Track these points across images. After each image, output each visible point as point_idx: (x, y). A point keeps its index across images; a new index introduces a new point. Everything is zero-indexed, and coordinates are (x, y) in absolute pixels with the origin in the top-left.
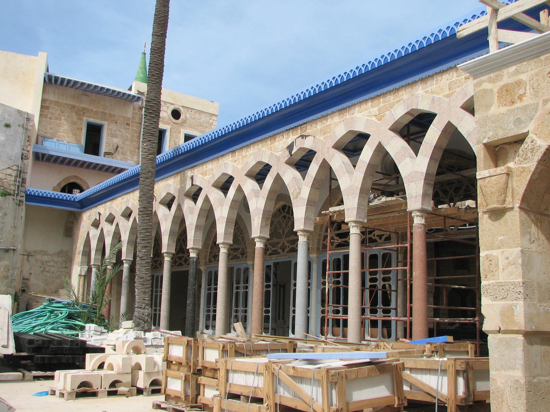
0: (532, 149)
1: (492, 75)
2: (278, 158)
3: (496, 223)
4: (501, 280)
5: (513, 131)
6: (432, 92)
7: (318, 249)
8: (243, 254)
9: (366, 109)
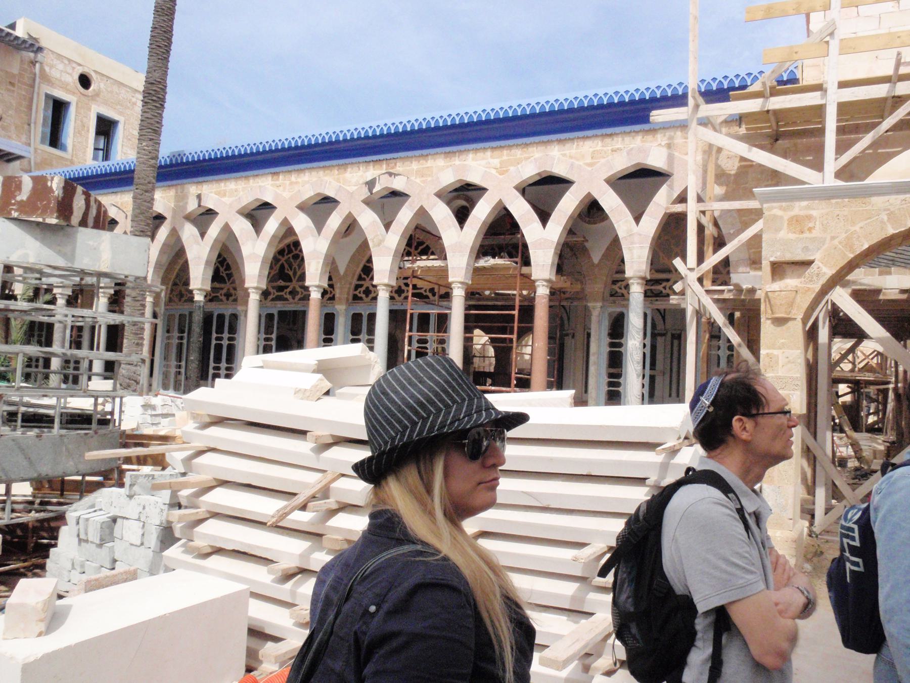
0: (818, 275)
1: (784, 204)
2: (351, 195)
3: (779, 329)
4: (780, 374)
5: (800, 256)
6: (571, 157)
7: (348, 300)
8: (228, 295)
9: (483, 159)
